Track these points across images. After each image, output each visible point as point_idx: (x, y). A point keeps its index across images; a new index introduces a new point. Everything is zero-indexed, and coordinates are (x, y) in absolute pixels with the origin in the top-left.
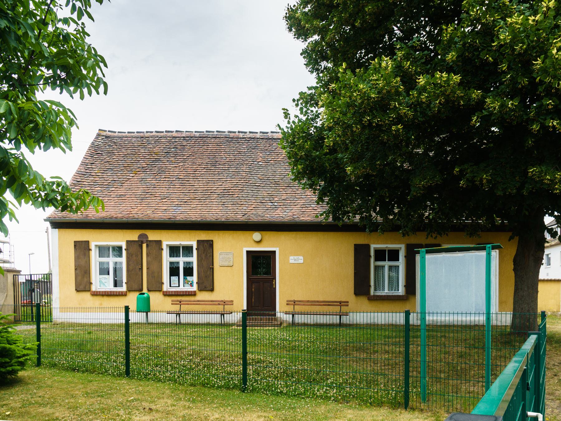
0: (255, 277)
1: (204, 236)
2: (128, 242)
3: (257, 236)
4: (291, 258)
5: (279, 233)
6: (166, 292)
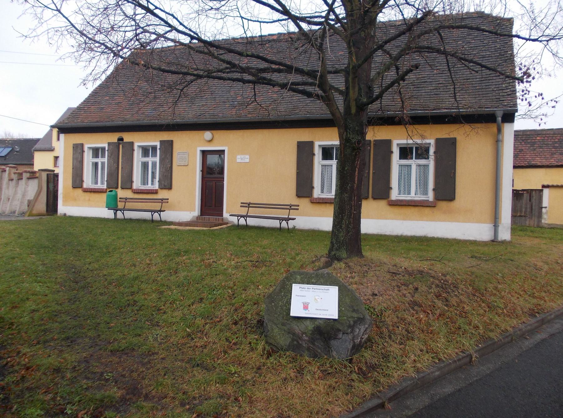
0: (209, 176)
1: (166, 136)
2: (109, 144)
3: (208, 135)
4: (239, 157)
5: (229, 131)
6: (137, 190)
